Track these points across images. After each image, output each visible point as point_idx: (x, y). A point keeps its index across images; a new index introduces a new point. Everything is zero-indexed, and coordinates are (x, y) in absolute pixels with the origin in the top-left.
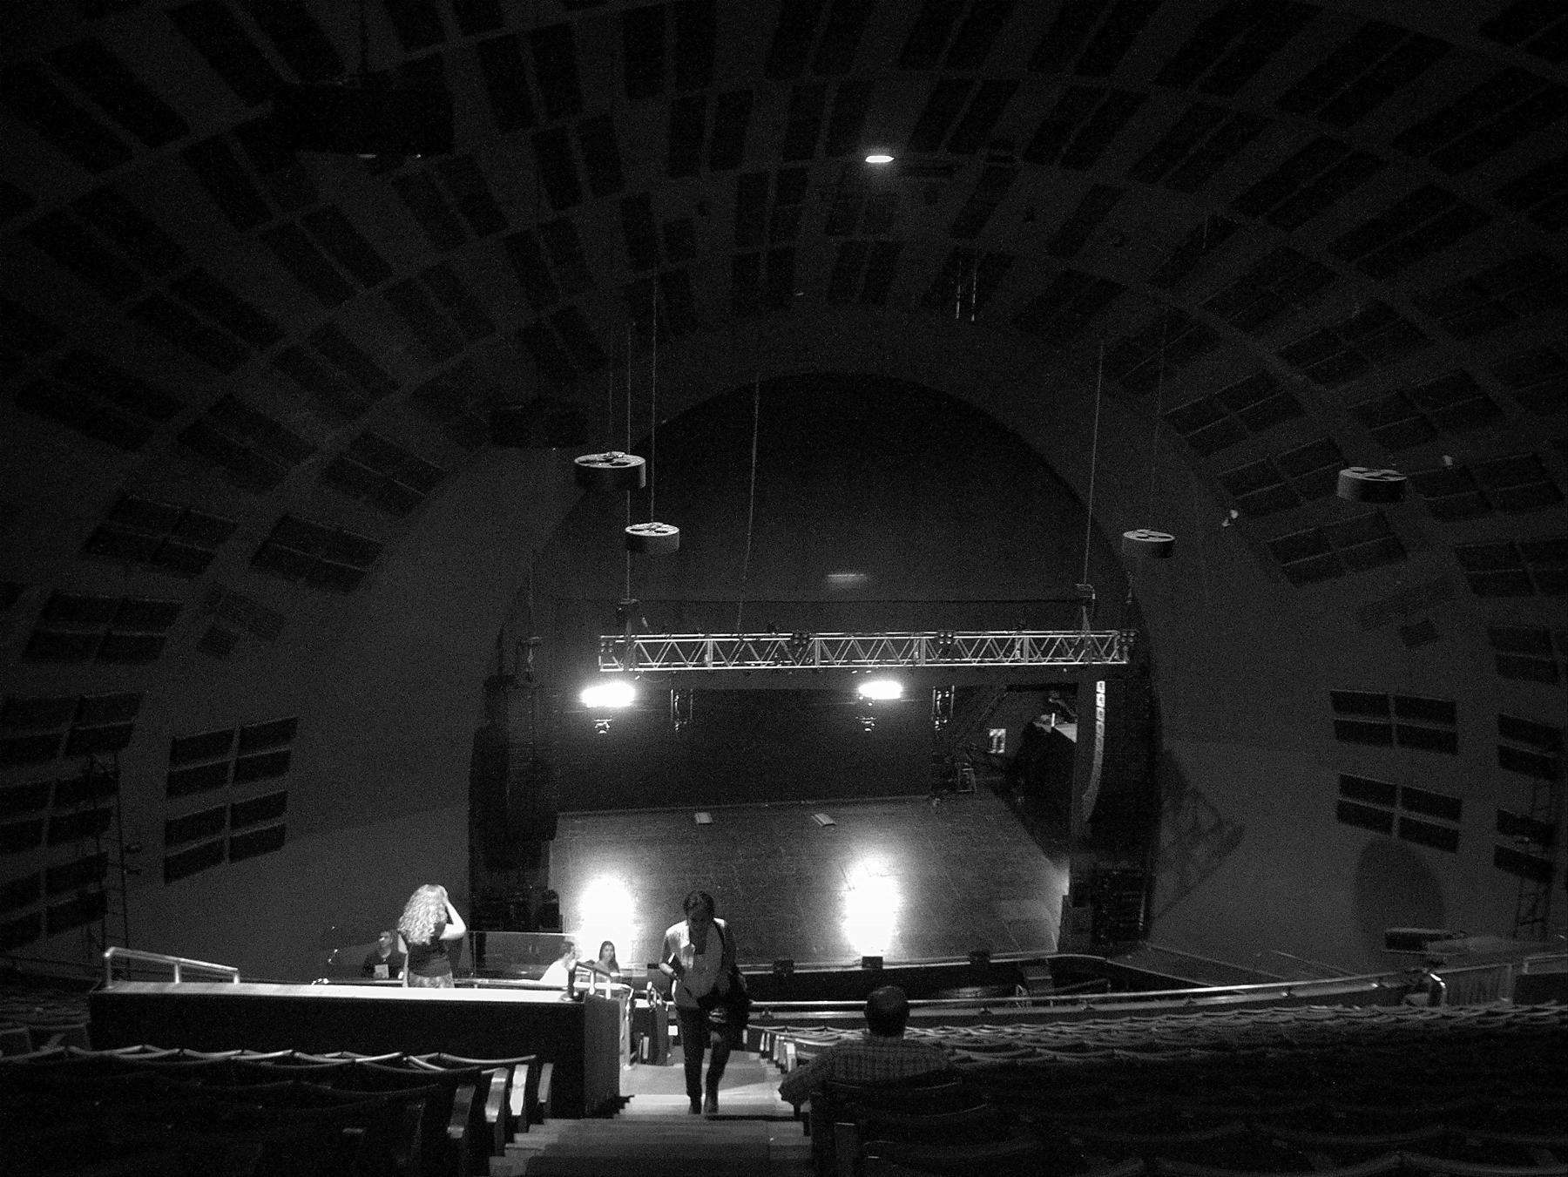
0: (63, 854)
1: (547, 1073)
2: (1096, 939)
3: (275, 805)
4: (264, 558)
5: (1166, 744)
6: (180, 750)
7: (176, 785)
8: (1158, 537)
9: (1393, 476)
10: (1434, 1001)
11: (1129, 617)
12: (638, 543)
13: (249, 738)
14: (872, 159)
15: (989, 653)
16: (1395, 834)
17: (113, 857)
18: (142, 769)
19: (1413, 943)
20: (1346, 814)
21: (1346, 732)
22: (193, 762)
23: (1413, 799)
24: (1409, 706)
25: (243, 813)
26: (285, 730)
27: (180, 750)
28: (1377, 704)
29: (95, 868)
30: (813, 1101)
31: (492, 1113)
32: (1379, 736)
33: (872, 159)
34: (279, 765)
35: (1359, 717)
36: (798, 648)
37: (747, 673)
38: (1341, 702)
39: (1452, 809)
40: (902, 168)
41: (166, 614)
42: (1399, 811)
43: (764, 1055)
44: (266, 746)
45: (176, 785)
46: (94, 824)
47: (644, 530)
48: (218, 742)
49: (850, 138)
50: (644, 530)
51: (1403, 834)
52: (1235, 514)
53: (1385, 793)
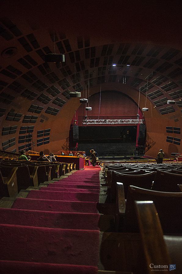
0: (23, 135)
1: (75, 165)
2: (139, 155)
3: (48, 138)
4: (46, 112)
5: (147, 133)
6: (38, 132)
7: (38, 136)
8: (146, 109)
9: (174, 101)
10: (177, 161)
11: (143, 118)
12: (87, 109)
13: (45, 131)
14: (113, 65)
15: (127, 122)
16: (173, 143)
17: (32, 144)
18: (34, 134)
19: (174, 155)
20: (167, 141)
21: (167, 131)
22: (40, 134)
23: (175, 139)
24: (175, 129)
25: (45, 139)
26: (49, 130)
27: (38, 132)
28: (171, 128)
29: (30, 145)
30: (125, 199)
31: (68, 168)
32: (171, 132)
33: (113, 65)
34: (49, 134)
35: (169, 130)
36: (105, 121)
37: (99, 124)
38: (167, 128)
39: (180, 140)
40: (117, 66)
41: (36, 118)
42: (173, 141)
43: (101, 166)
44: (47, 132)
45: (38, 136)
46: (30, 140)
47: (88, 108)
48: (42, 132)
49: (111, 63)
50: (88, 108)
51: (174, 143)
52: (155, 106)
53: (172, 139)
